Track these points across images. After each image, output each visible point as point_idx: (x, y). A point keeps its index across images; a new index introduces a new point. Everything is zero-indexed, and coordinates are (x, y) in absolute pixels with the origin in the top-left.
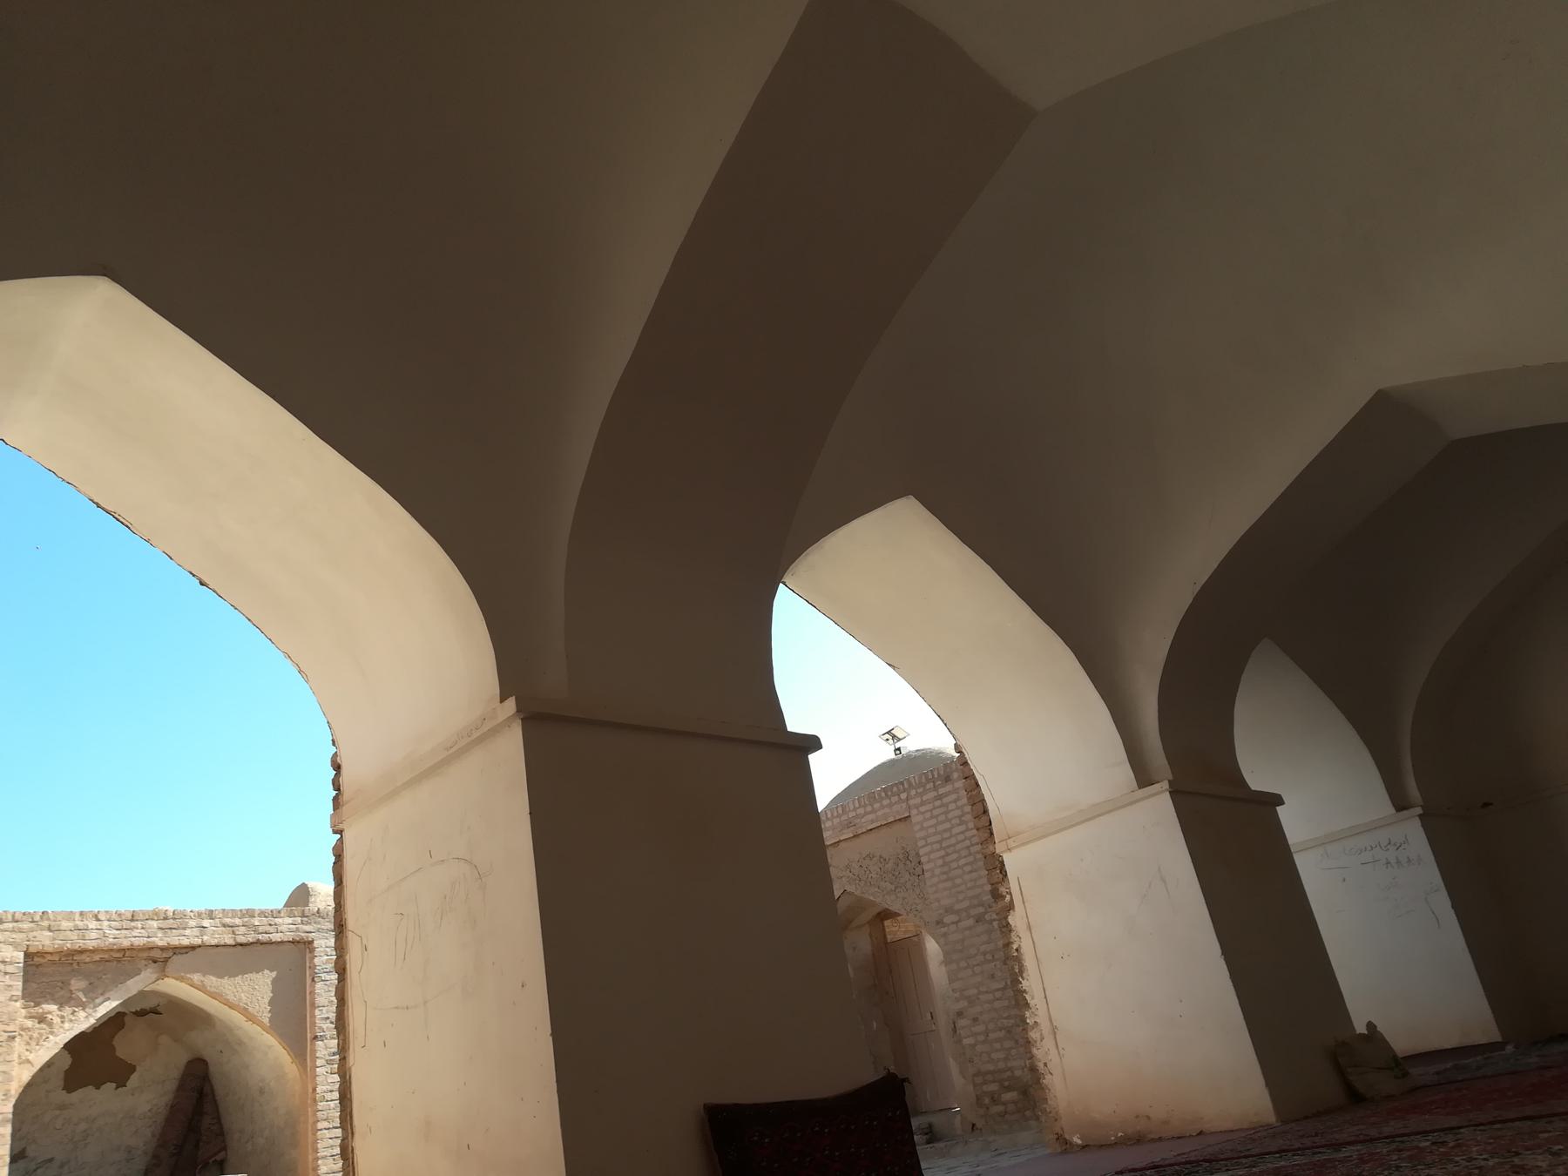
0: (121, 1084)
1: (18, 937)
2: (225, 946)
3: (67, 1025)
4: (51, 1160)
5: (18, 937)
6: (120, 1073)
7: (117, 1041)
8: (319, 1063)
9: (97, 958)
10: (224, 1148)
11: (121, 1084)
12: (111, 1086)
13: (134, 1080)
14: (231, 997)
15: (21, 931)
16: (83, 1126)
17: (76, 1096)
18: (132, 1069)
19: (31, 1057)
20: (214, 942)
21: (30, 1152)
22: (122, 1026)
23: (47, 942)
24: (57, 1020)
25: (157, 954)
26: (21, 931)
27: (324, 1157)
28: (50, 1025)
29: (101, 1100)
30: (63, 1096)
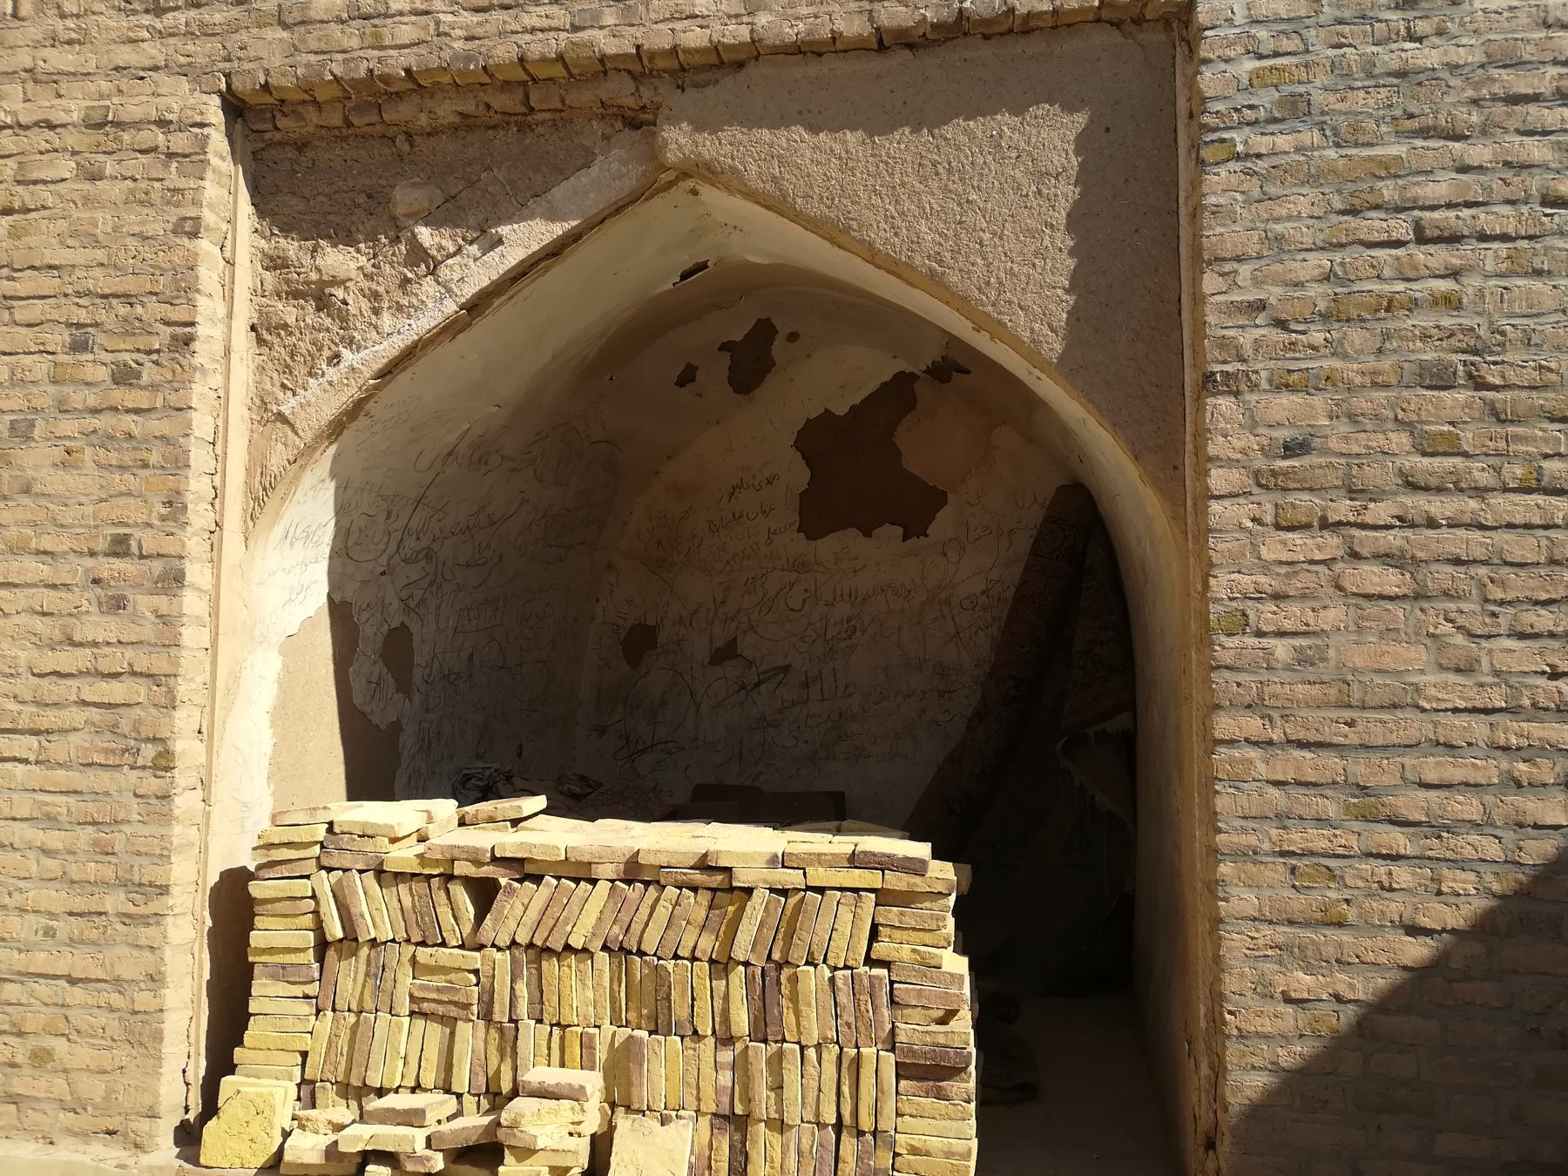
0: (915, 527)
1: (202, 50)
2: (836, 46)
3: (387, 321)
4: (786, 669)
5: (202, 50)
6: (913, 507)
7: (904, 436)
8: (1218, 479)
9: (446, 111)
10: (1132, 706)
11: (915, 527)
12: (891, 532)
13: (943, 523)
14: (879, 235)
15: (207, 32)
16: (842, 610)
17: (827, 547)
18: (940, 499)
19: (288, 405)
20: (791, 32)
21: (747, 646)
22: (909, 404)
23: (276, 61)
24: (358, 305)
25: (620, 91)
26: (207, 32)
27: (1240, 854)
28: (343, 319)
29: (870, 560)
30: (796, 544)
